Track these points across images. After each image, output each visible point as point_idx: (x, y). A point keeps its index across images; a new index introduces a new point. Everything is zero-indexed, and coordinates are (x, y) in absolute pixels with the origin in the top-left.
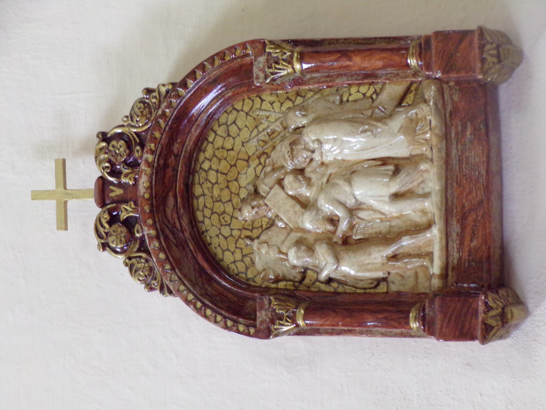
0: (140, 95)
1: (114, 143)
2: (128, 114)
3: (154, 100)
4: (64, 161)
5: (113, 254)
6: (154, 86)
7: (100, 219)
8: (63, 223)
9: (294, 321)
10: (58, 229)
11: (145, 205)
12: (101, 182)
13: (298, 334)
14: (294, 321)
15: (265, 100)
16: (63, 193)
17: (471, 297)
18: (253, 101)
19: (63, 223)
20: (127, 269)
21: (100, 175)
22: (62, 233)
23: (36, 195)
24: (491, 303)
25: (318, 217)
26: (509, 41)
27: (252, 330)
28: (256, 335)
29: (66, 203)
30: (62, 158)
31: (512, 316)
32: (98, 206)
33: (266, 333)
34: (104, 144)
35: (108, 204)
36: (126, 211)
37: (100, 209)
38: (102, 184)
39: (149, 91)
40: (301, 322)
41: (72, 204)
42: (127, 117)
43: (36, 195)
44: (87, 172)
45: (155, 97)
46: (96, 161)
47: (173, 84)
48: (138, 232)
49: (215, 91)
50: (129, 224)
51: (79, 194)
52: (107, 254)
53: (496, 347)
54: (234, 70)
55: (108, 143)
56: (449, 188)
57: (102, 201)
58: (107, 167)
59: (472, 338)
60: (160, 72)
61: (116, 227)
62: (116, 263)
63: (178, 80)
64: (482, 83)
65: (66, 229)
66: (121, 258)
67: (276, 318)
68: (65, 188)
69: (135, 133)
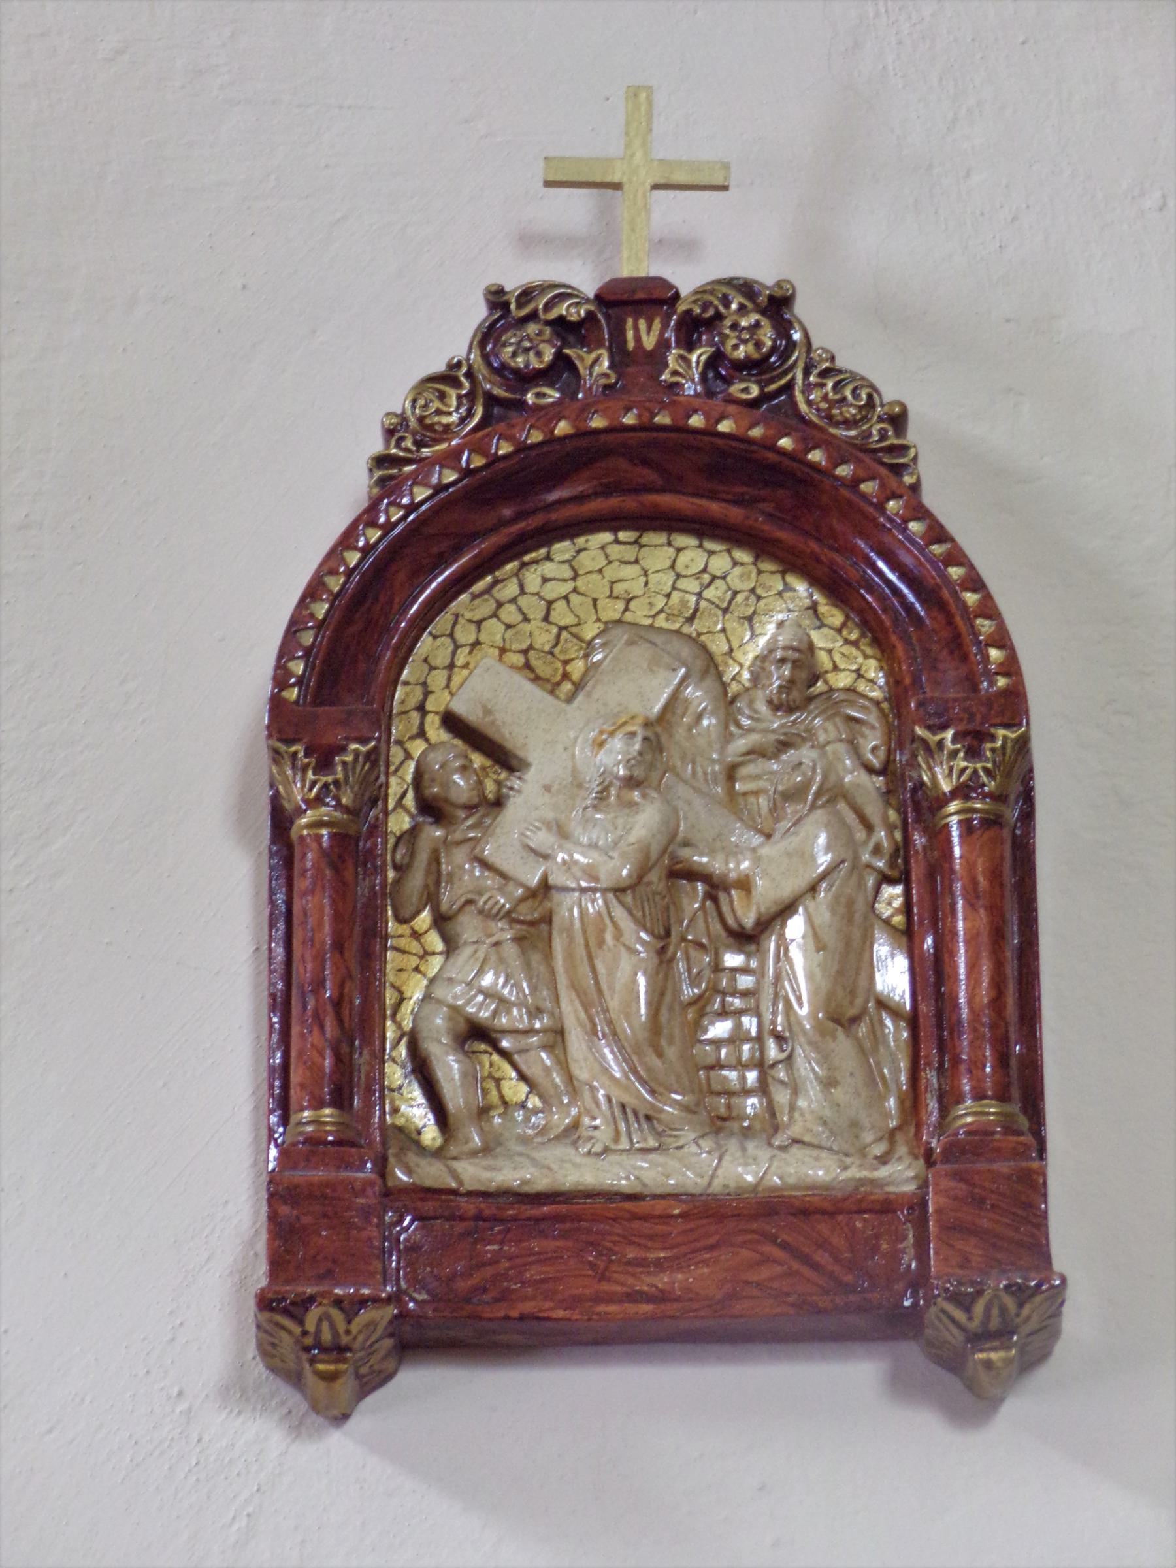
0: (890, 393)
2: (840, 363)
4: (725, 188)
20: (439, 367)
21: (684, 292)
22: (539, 173)
23: (639, 96)
24: (365, 1315)
25: (464, 369)
30: (732, 184)
36: (596, 364)
38: (651, 297)
39: (898, 420)
42: (833, 359)
43: (639, 96)
44: (702, 249)
45: (883, 436)
46: (713, 282)
56: (684, 1325)
59: (278, 1264)
65: (548, 184)
67: (324, 760)
68: (656, 187)
69: (793, 378)
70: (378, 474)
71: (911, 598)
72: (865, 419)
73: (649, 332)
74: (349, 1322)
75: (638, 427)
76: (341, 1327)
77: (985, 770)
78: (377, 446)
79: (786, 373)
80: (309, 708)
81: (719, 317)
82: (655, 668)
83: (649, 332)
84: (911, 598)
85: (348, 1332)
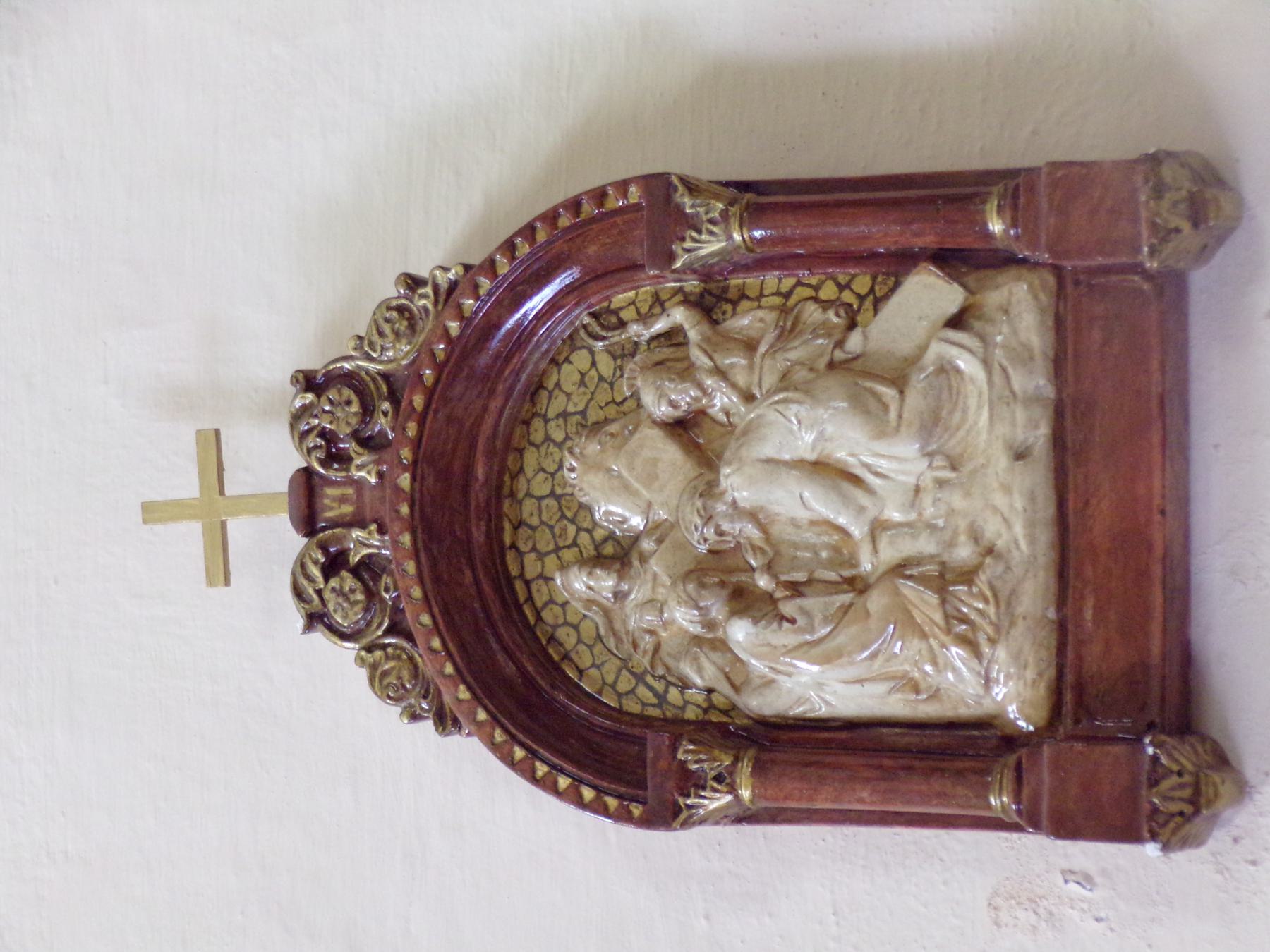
0: (391, 290)
1: (332, 394)
3: (422, 302)
4: (217, 432)
5: (335, 639)
6: (424, 273)
7: (303, 566)
8: (220, 569)
9: (732, 789)
10: (211, 583)
11: (401, 533)
12: (302, 479)
13: (739, 820)
14: (732, 789)
15: (570, 363)
16: (214, 504)
17: (1114, 741)
18: (584, 347)
19: (220, 569)
20: (363, 673)
23: (153, 512)
26: (1220, 182)
27: (637, 810)
28: (647, 822)
29: (223, 525)
31: (1217, 795)
32: (297, 529)
33: (665, 815)
34: (310, 397)
35: (323, 529)
37: (306, 540)
38: (307, 487)
39: (413, 283)
40: (746, 794)
41: (239, 529)
43: (153, 512)
44: (270, 458)
47: (467, 268)
48: (387, 590)
49: (558, 280)
50: (368, 570)
51: (256, 504)
52: (319, 638)
53: (1187, 864)
54: (602, 235)
55: (319, 396)
57: (308, 522)
58: (316, 447)
60: (435, 248)
61: (334, 581)
62: (340, 663)
63: (476, 260)
64: (336, 466)
65: (227, 582)
66: (349, 650)
67: (691, 782)
68: (222, 492)
70: (449, 727)
71: (548, 293)
72: (410, 311)
73: (415, 645)
74: (1172, 772)
75: (443, 510)
76: (1174, 780)
77: (707, 213)
78: (428, 725)
79: (373, 379)
80: (649, 793)
81: (323, 434)
82: (717, 491)
83: (415, 645)
84: (548, 293)
85: (1180, 774)
